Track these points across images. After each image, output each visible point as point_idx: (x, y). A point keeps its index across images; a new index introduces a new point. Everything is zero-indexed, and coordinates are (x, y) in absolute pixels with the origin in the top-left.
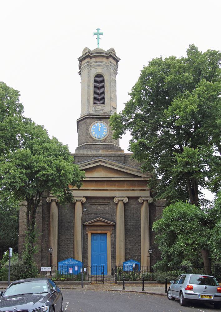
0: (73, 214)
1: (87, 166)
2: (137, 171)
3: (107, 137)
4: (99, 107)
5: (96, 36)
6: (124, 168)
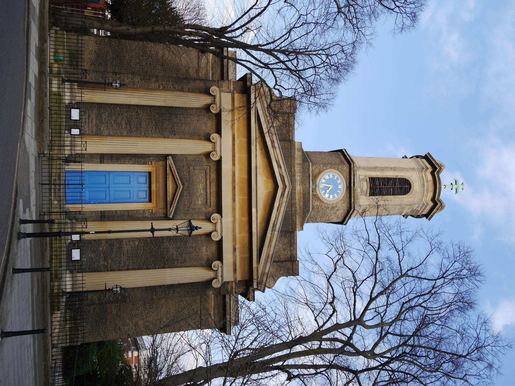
1: (275, 162)
3: (320, 200)
4: (365, 186)
6: (273, 230)
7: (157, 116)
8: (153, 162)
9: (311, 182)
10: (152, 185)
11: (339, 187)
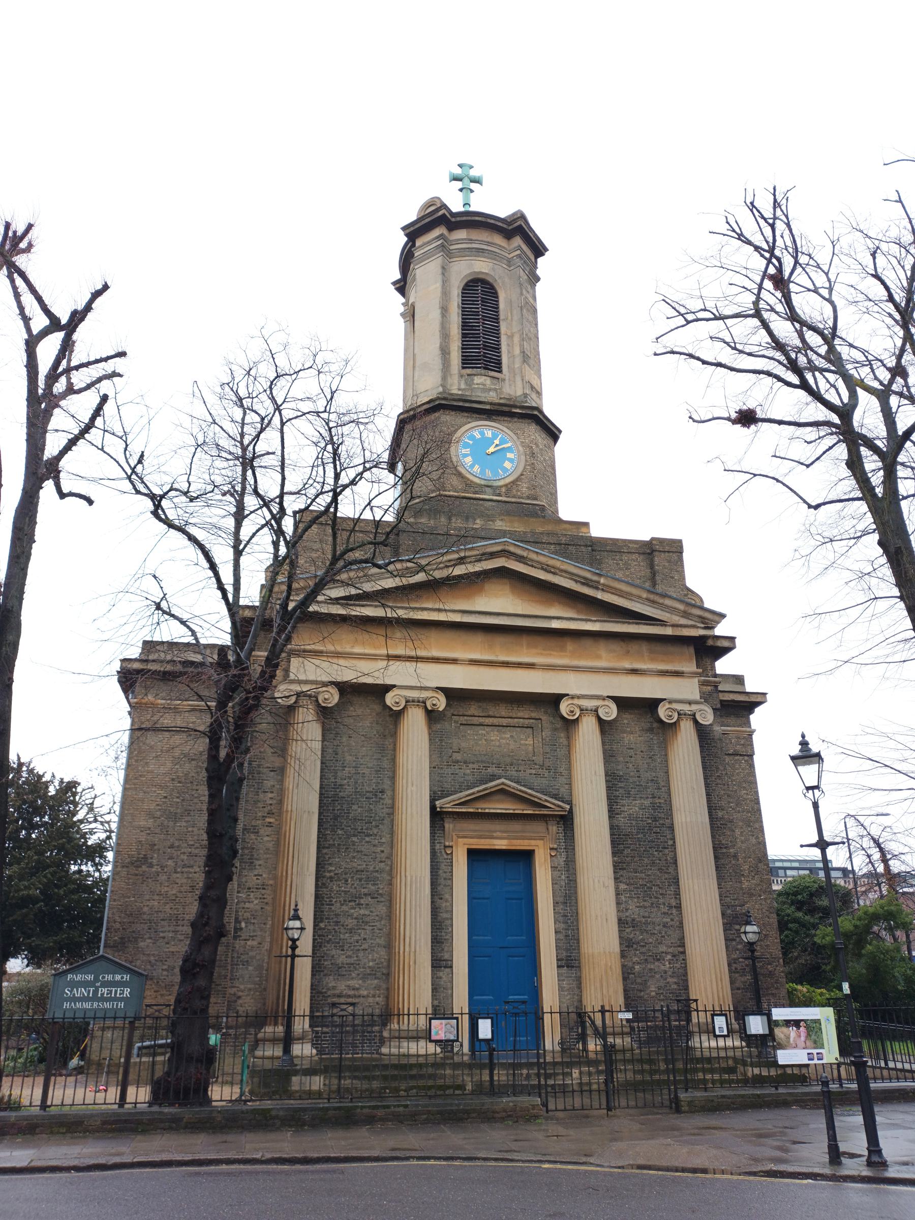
0: (386, 764)
2: (648, 599)
3: (518, 479)
5: (459, 185)
6: (595, 586)
7: (340, 832)
8: (447, 844)
9: (481, 496)
10: (497, 847)
11: (490, 435)
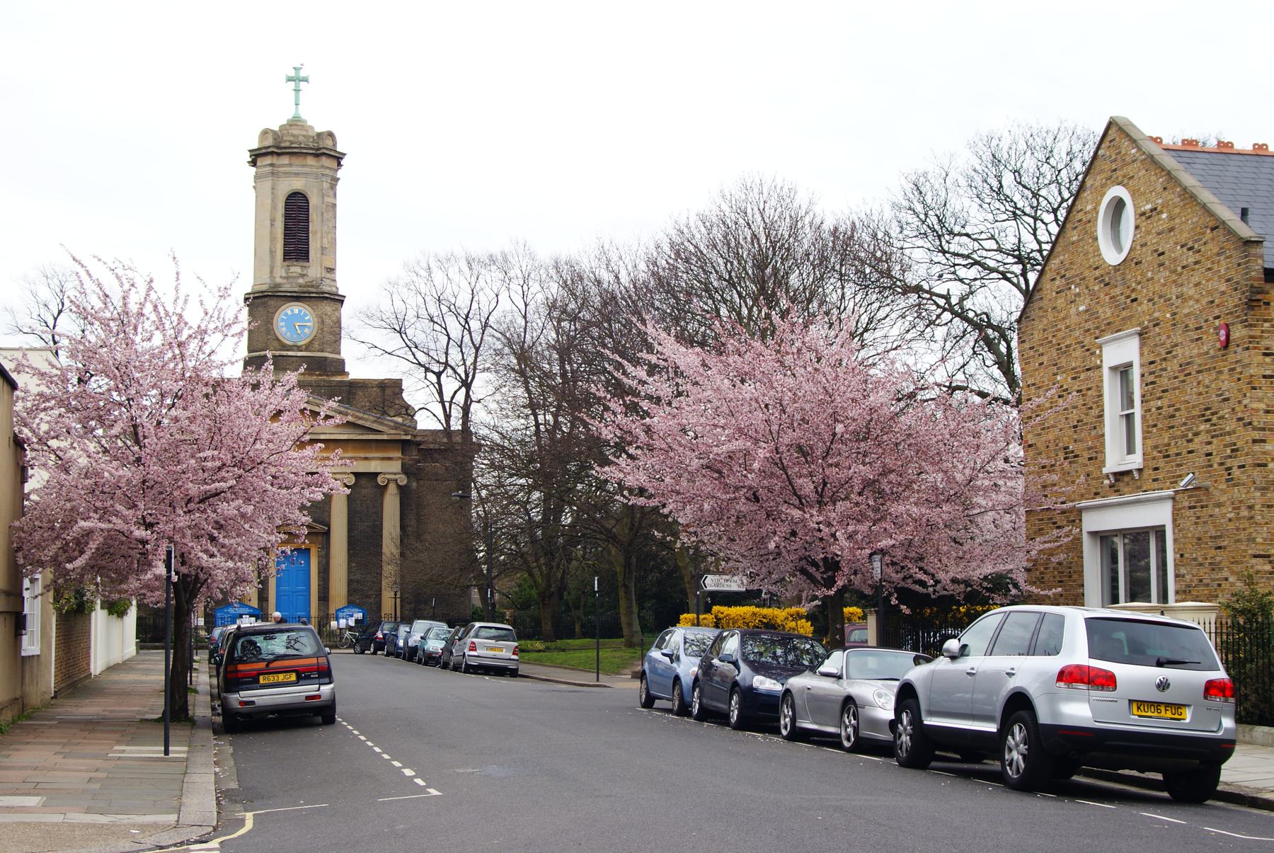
3: (312, 340)
4: (296, 269)
